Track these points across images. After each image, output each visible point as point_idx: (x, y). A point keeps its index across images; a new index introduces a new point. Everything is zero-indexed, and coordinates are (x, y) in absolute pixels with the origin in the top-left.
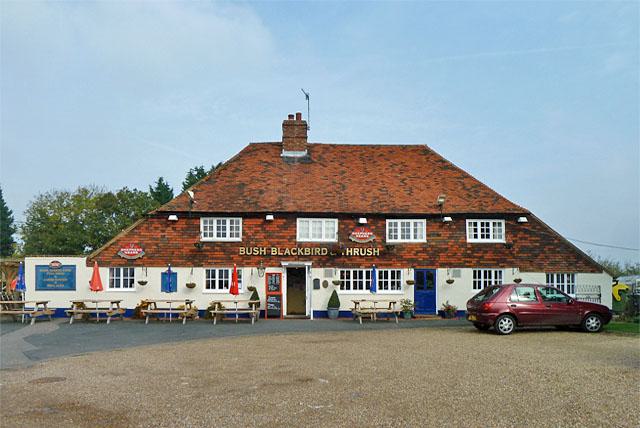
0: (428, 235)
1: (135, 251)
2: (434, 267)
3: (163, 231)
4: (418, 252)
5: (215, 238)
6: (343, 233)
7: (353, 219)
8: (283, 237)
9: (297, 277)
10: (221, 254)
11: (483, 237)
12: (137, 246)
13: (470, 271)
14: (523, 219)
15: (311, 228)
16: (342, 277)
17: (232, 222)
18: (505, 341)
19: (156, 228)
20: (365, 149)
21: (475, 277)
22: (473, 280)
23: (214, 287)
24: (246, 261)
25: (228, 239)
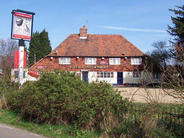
0: (121, 63)
3: (49, 61)
4: (118, 67)
6: (98, 62)
8: (81, 63)
19: (47, 61)
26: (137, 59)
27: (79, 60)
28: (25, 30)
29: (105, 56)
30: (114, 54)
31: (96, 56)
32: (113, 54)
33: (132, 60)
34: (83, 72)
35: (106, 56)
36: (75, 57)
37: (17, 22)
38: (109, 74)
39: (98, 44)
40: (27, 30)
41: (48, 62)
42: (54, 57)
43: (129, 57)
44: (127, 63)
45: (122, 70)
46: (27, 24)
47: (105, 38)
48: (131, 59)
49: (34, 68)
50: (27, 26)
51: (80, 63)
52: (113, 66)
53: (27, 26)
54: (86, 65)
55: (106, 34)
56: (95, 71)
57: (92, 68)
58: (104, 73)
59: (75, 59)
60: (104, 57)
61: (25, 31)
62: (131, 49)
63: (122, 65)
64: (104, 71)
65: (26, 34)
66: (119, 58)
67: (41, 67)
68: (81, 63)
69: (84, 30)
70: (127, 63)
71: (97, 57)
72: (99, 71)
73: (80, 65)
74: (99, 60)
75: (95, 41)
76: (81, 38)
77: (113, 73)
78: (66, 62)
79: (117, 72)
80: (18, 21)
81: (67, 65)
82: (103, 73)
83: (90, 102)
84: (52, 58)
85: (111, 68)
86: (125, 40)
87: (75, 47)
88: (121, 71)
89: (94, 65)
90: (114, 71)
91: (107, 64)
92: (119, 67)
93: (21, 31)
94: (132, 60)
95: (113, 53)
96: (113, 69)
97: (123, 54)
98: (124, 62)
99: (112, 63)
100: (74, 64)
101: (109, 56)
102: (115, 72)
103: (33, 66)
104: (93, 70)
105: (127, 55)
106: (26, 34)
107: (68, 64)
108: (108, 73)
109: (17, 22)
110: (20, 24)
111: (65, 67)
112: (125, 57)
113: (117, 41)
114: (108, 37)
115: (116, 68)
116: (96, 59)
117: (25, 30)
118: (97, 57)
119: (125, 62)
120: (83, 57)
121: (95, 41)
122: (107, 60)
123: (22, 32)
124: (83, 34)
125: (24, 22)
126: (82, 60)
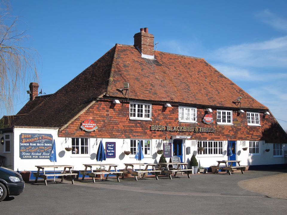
0: (233, 120)
1: (92, 125)
2: (236, 140)
3: (107, 111)
4: (230, 130)
5: (136, 118)
6: (201, 119)
7: (203, 108)
8: (171, 119)
9: (178, 144)
10: (140, 130)
11: (138, 116)
12: (93, 121)
13: (248, 141)
14: (268, 113)
15: (144, 111)
16: (73, 144)
17: (253, 115)
18: (259, 172)
19: (103, 109)
20: (141, 64)
21: (132, 146)
22: (259, 147)
23: (206, 153)
24: (153, 134)
25: (144, 118)
26: (183, 109)
33: (180, 110)
36: (162, 104)
38: (216, 145)
45: (235, 137)
49: (74, 128)
54: (180, 124)
59: (161, 107)
79: (227, 141)
83: (264, 122)
85: (220, 132)
94: (180, 110)
96: (223, 135)
102: (225, 141)
103: (72, 123)
111: (142, 127)
116: (196, 109)
118: (154, 103)
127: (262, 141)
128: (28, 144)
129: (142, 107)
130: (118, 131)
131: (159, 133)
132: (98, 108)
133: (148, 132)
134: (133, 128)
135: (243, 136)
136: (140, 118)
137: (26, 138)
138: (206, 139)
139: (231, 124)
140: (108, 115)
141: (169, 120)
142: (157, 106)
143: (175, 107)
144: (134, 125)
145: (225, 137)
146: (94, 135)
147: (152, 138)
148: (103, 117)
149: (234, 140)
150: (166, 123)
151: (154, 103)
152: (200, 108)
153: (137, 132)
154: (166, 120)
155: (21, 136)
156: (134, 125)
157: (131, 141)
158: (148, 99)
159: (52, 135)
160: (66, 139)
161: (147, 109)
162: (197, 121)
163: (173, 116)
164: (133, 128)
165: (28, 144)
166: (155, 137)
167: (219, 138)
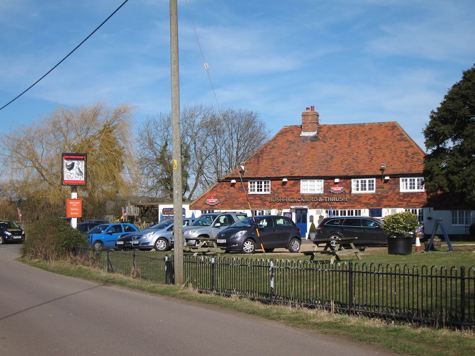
0: (377, 188)
3: (229, 189)
4: (370, 199)
5: (256, 192)
6: (327, 188)
8: (293, 191)
10: (259, 202)
12: (215, 197)
19: (225, 187)
25: (263, 192)
26: (406, 180)
27: (287, 185)
28: (77, 174)
29: (343, 174)
30: (363, 170)
31: (323, 174)
32: (362, 169)
34: (297, 210)
35: (345, 174)
37: (67, 166)
39: (336, 146)
40: (79, 173)
41: (227, 191)
42: (238, 179)
43: (396, 177)
44: (390, 189)
45: (379, 205)
46: (80, 166)
47: (355, 131)
48: (401, 179)
50: (79, 169)
51: (290, 191)
52: (359, 196)
53: (79, 169)
54: (303, 195)
55: (362, 122)
56: (322, 207)
57: (315, 201)
58: (341, 212)
60: (340, 177)
61: (77, 175)
62: (407, 156)
63: (379, 193)
64: (340, 209)
65: (79, 178)
66: (373, 179)
67: (214, 201)
68: (293, 191)
69: (311, 117)
70: (390, 189)
71: (326, 178)
72: (329, 208)
73: (291, 195)
74: (329, 183)
75: (333, 141)
76: (303, 134)
77: (360, 211)
78: (263, 190)
80: (68, 164)
81: (263, 196)
82: (337, 211)
84: (233, 181)
85: (356, 201)
86: (402, 135)
87: (286, 155)
88: (378, 208)
89: (319, 195)
90: (362, 207)
91: (347, 191)
92: (372, 198)
93: (72, 176)
95: (360, 168)
96: (360, 203)
97: (382, 170)
98: (383, 188)
99: (358, 189)
100: (278, 193)
101: (351, 174)
104: (318, 204)
105: (391, 172)
106: (79, 178)
107: (267, 193)
108: (349, 211)
109: (67, 166)
110: (71, 167)
111: (261, 200)
112: (385, 176)
113: (381, 138)
114: (363, 129)
115: (366, 201)
117: (77, 174)
118: (273, 179)
119: (387, 187)
120: (297, 179)
121: (333, 141)
122: (347, 184)
123: (74, 177)
124: (308, 126)
125: (76, 165)
126: (294, 185)
127: (428, 208)
128: (168, 215)
129: (261, 183)
130: (238, 204)
131: (279, 203)
132: (220, 187)
133: (267, 203)
134: (252, 201)
135: (391, 203)
136: (260, 193)
137: (167, 211)
138: (336, 207)
139: (374, 191)
140: (229, 192)
141: (289, 193)
142: (277, 181)
143: (297, 181)
144: (253, 198)
145: (363, 205)
146: (217, 207)
147: (271, 209)
148: (225, 193)
149: (380, 208)
150: (286, 195)
151: (273, 179)
152: (327, 179)
153: (256, 204)
154: (287, 193)
155: (163, 210)
156: (253, 198)
157: (360, 214)
158: (265, 177)
159: (425, 128)
160: (441, 274)
161: (260, 185)
162: (429, 179)
163: (294, 188)
164: (252, 201)
165: (168, 215)
166: (274, 207)
167: (354, 207)
